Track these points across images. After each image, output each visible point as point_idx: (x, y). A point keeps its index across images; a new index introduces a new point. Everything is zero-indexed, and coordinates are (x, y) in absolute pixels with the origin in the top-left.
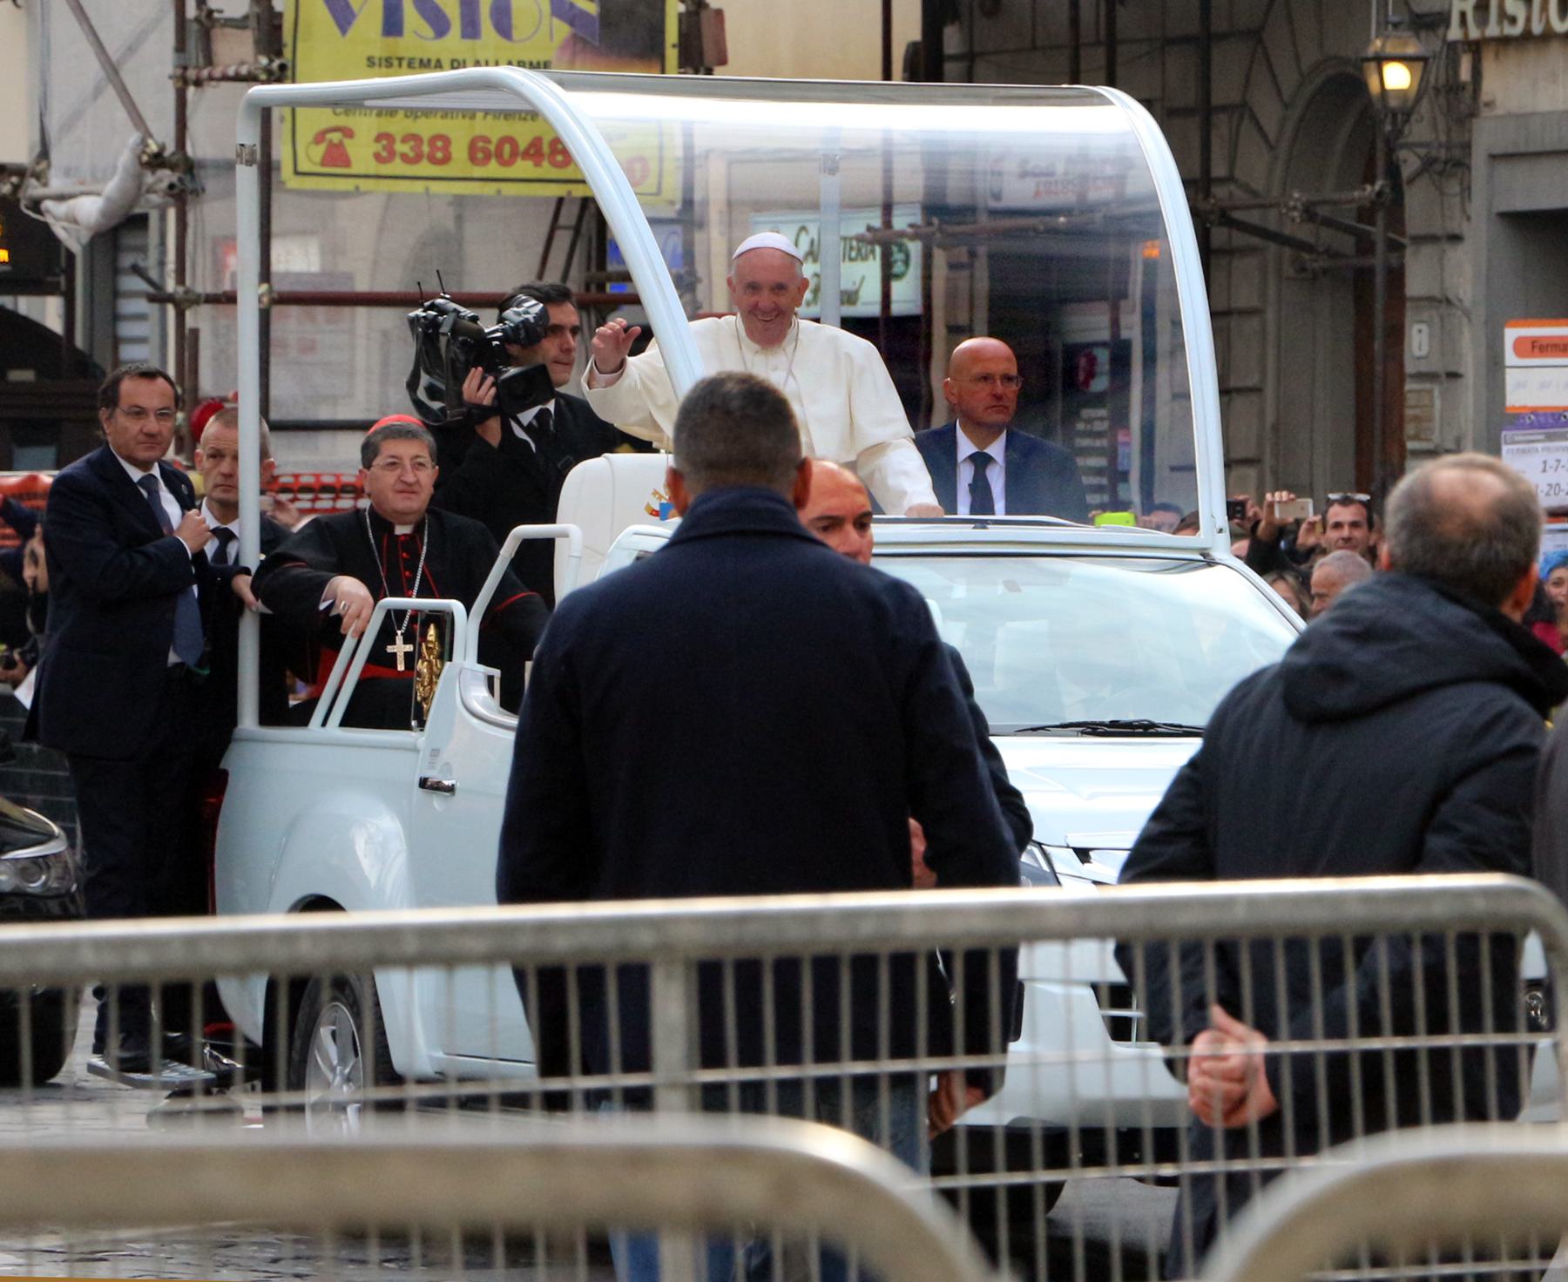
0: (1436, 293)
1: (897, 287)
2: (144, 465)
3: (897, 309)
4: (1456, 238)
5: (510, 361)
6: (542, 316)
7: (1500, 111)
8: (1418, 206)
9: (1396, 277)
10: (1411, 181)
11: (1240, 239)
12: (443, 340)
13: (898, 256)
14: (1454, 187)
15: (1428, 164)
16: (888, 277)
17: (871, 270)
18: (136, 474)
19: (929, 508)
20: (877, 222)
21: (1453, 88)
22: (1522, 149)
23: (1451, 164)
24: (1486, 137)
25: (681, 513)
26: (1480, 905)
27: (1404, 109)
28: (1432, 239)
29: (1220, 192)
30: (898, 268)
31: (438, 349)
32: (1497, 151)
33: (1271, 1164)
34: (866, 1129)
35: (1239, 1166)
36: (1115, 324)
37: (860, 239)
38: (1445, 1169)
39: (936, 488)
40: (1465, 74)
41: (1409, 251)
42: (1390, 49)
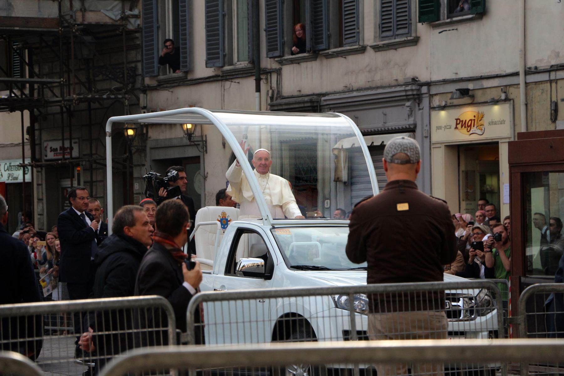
0: (140, 176)
1: (26, 176)
2: (81, 211)
3: (26, 181)
4: (144, 165)
5: (169, 186)
6: (177, 174)
7: (152, 139)
8: (136, 158)
9: (131, 173)
10: (134, 153)
11: (98, 166)
12: (153, 181)
13: (26, 169)
14: (143, 155)
15: (137, 150)
16: (24, 174)
17: (21, 172)
18: (79, 213)
19: (299, 216)
20: (22, 162)
21: (142, 134)
22: (157, 146)
23: (142, 150)
24: (149, 144)
25: (351, 220)
26: (152, 302)
27: (132, 138)
28: (139, 165)
29: (94, 156)
30: (26, 172)
31: (152, 184)
32: (152, 147)
33: (109, 357)
34: (23, 353)
35: (102, 357)
36: (72, 184)
37: (18, 166)
38: (146, 356)
39: (302, 212)
40: (145, 131)
41: (134, 168)
42: (129, 127)
